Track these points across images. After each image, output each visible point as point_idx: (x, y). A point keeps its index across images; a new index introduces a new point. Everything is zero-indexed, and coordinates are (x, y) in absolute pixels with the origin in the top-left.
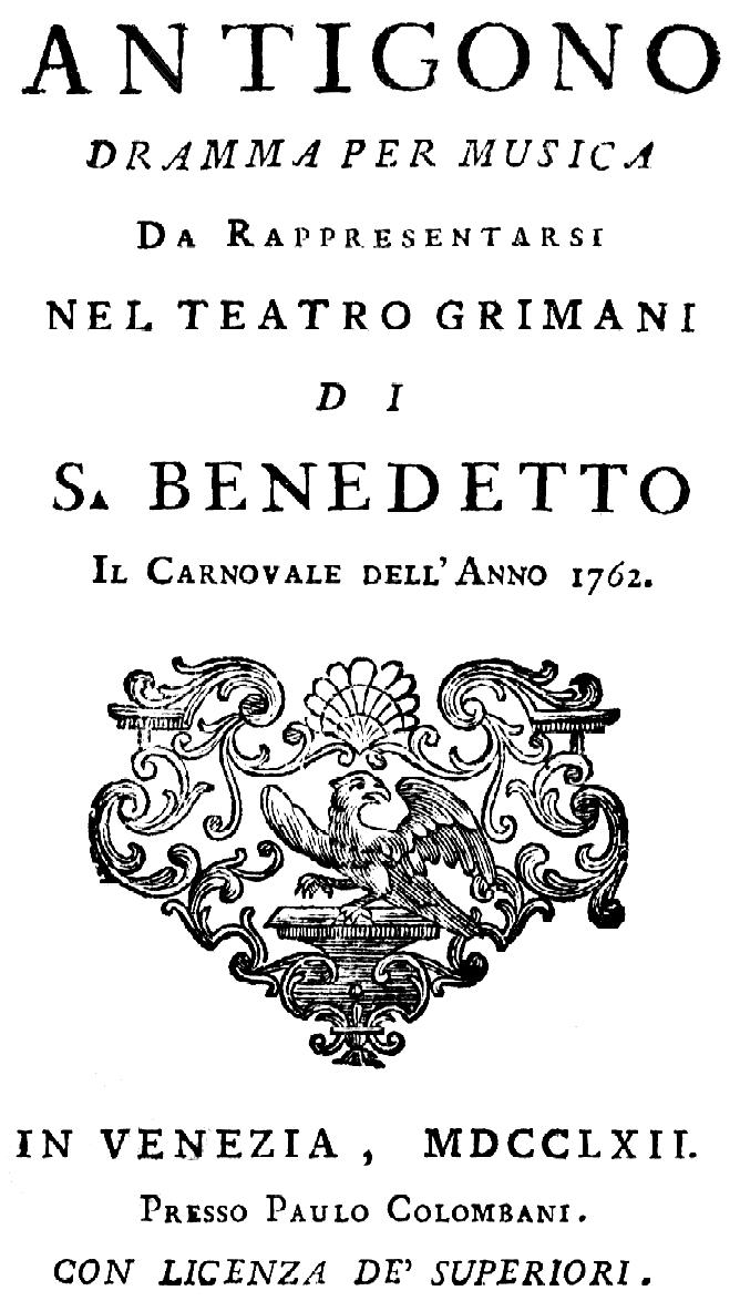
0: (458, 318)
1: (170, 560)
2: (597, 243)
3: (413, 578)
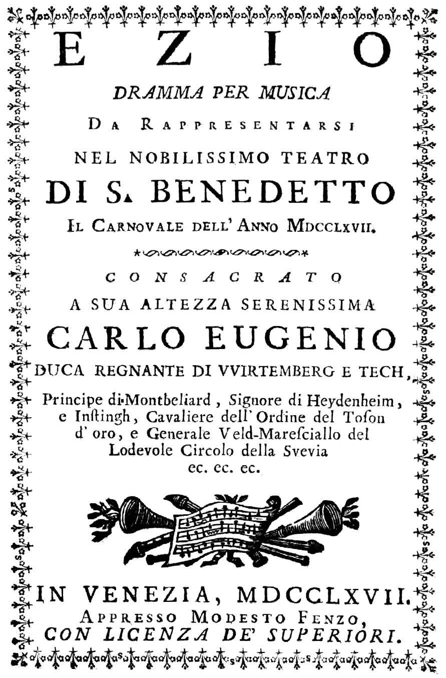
1: (103, 220)
3: (339, 229)
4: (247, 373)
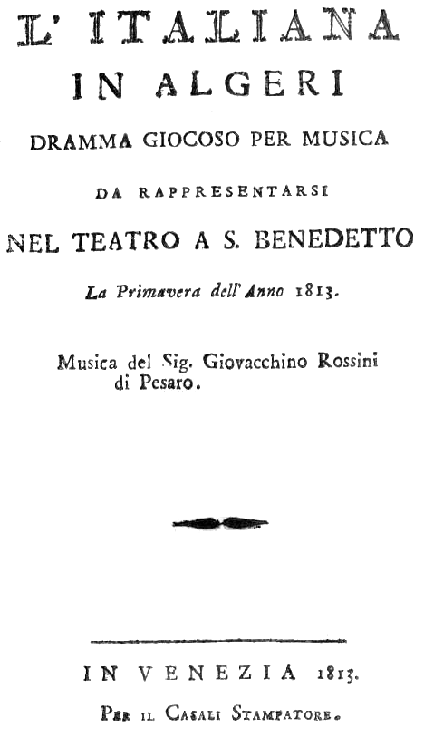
0: (246, 87)
2: (299, 289)
4: (321, 136)
